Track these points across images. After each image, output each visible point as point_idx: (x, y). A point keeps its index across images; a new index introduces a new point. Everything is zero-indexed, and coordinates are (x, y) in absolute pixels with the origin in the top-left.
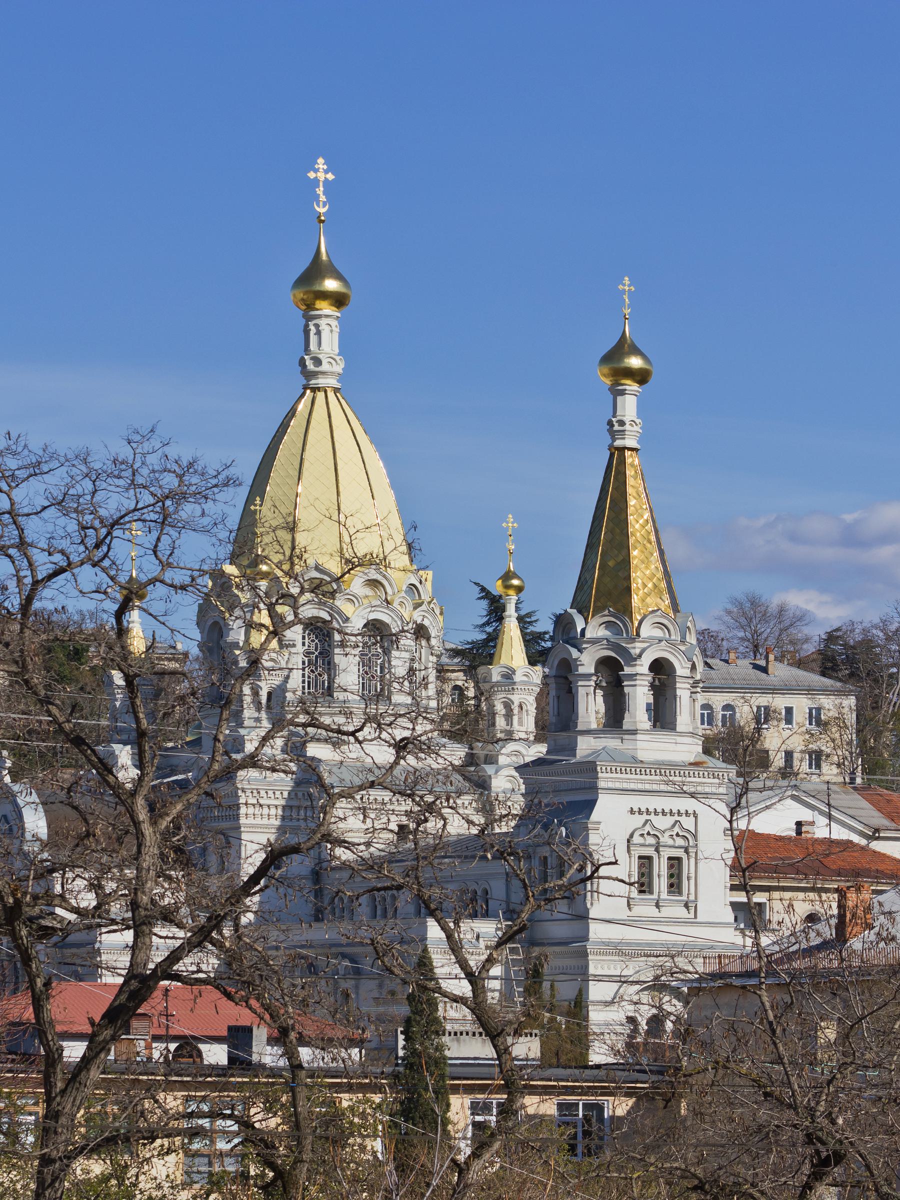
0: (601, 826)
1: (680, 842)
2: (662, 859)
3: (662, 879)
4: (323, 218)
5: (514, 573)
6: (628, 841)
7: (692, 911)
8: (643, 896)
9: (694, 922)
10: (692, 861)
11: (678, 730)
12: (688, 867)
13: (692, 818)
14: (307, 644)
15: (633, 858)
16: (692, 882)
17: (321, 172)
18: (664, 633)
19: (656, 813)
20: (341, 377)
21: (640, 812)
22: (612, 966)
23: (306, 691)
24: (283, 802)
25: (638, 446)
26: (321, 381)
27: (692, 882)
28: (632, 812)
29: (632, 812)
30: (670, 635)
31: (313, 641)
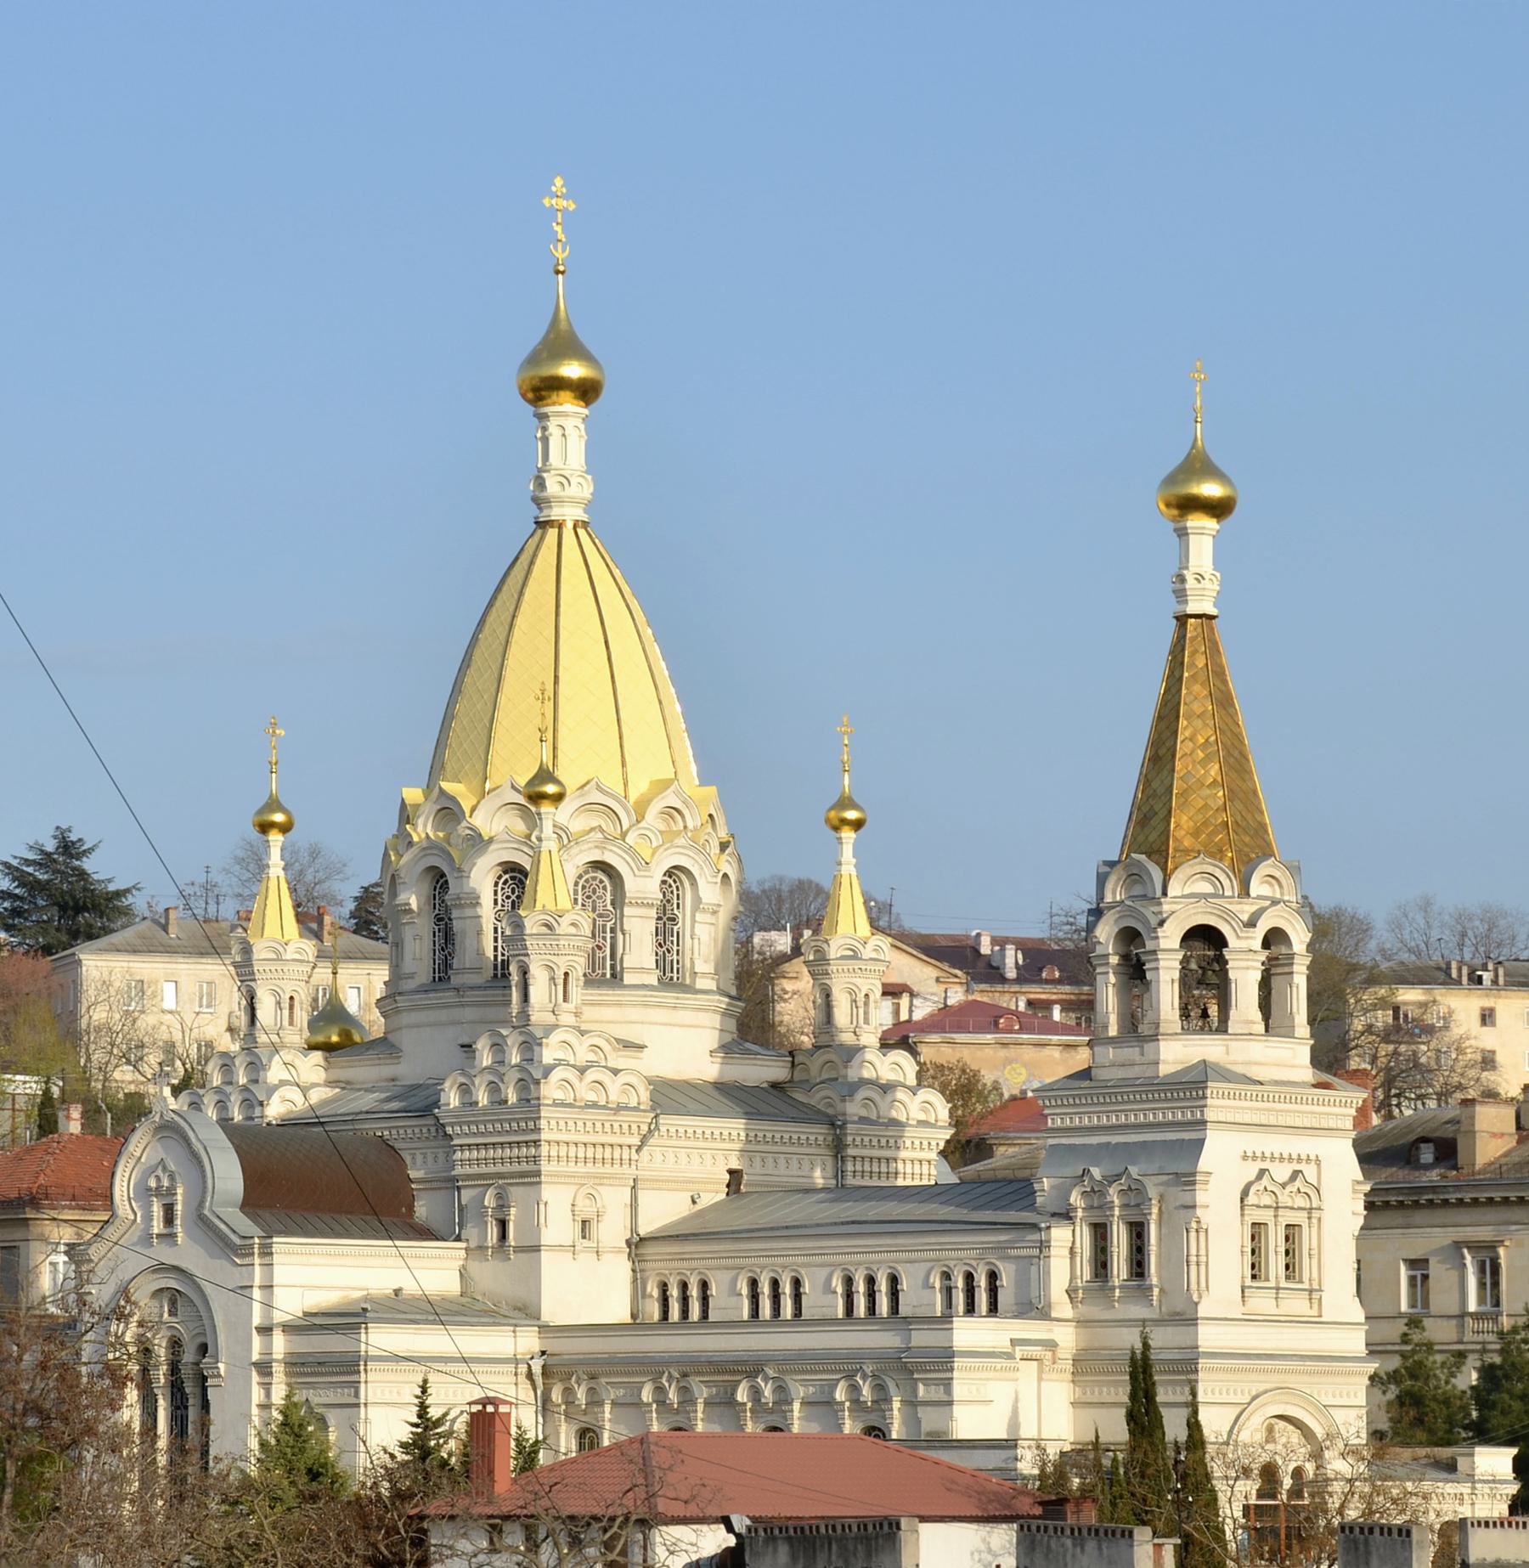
0: (1212, 1179)
1: (1301, 1202)
2: (1279, 1227)
3: (1279, 1257)
4: (561, 268)
5: (850, 799)
6: (1242, 1200)
7: (1316, 1306)
8: (1255, 1284)
9: (1317, 1322)
10: (1314, 1230)
11: (1230, 1031)
12: (1307, 1239)
13: (1313, 1167)
14: (500, 901)
15: (1245, 1226)
16: (1315, 1262)
17: (559, 198)
18: (1274, 891)
19: (1273, 1158)
20: (589, 507)
21: (1254, 1158)
22: (1096, 1390)
23: (437, 975)
24: (738, 1146)
25: (1213, 611)
26: (555, 513)
27: (1203, 1268)
28: (1245, 1157)
29: (1245, 1157)
30: (1282, 894)
31: (508, 897)
